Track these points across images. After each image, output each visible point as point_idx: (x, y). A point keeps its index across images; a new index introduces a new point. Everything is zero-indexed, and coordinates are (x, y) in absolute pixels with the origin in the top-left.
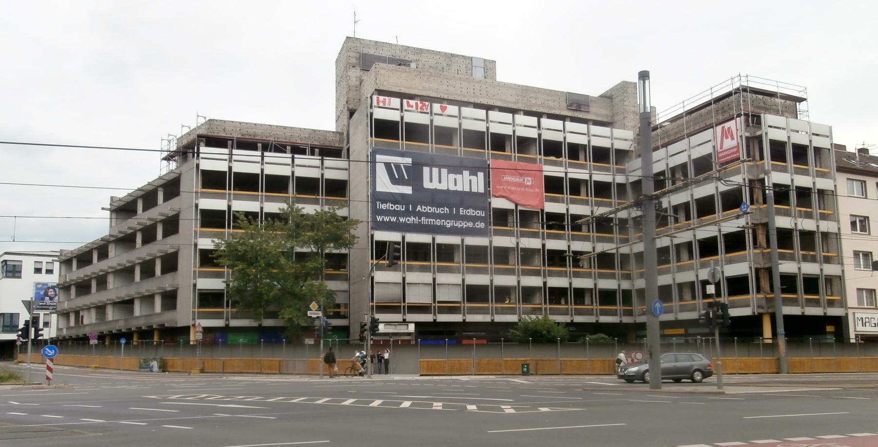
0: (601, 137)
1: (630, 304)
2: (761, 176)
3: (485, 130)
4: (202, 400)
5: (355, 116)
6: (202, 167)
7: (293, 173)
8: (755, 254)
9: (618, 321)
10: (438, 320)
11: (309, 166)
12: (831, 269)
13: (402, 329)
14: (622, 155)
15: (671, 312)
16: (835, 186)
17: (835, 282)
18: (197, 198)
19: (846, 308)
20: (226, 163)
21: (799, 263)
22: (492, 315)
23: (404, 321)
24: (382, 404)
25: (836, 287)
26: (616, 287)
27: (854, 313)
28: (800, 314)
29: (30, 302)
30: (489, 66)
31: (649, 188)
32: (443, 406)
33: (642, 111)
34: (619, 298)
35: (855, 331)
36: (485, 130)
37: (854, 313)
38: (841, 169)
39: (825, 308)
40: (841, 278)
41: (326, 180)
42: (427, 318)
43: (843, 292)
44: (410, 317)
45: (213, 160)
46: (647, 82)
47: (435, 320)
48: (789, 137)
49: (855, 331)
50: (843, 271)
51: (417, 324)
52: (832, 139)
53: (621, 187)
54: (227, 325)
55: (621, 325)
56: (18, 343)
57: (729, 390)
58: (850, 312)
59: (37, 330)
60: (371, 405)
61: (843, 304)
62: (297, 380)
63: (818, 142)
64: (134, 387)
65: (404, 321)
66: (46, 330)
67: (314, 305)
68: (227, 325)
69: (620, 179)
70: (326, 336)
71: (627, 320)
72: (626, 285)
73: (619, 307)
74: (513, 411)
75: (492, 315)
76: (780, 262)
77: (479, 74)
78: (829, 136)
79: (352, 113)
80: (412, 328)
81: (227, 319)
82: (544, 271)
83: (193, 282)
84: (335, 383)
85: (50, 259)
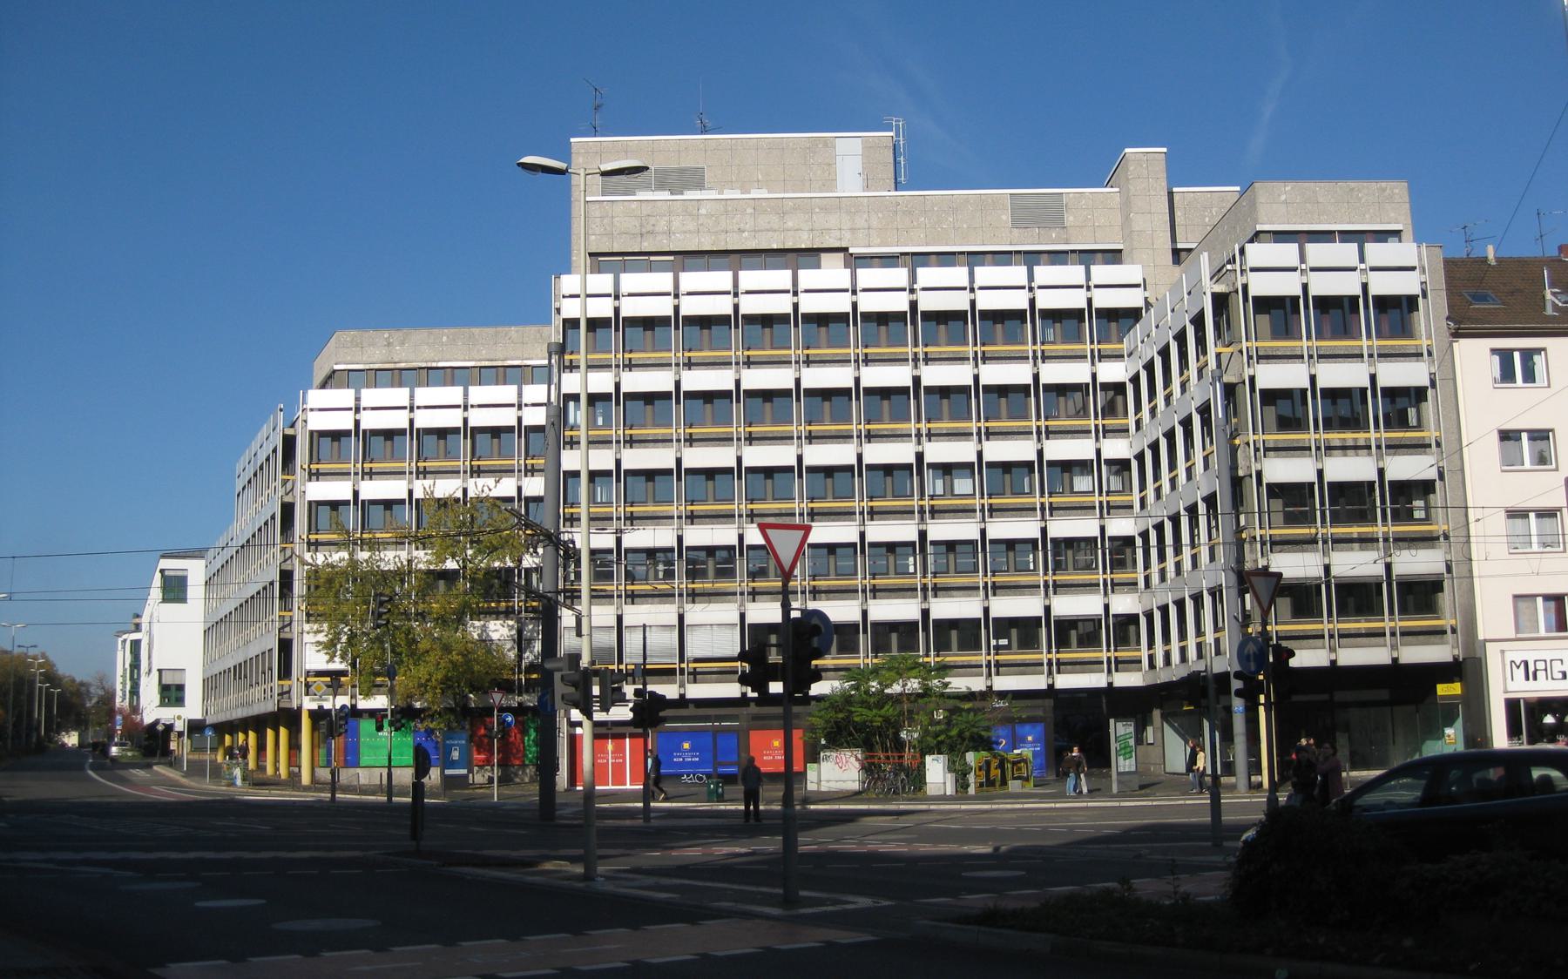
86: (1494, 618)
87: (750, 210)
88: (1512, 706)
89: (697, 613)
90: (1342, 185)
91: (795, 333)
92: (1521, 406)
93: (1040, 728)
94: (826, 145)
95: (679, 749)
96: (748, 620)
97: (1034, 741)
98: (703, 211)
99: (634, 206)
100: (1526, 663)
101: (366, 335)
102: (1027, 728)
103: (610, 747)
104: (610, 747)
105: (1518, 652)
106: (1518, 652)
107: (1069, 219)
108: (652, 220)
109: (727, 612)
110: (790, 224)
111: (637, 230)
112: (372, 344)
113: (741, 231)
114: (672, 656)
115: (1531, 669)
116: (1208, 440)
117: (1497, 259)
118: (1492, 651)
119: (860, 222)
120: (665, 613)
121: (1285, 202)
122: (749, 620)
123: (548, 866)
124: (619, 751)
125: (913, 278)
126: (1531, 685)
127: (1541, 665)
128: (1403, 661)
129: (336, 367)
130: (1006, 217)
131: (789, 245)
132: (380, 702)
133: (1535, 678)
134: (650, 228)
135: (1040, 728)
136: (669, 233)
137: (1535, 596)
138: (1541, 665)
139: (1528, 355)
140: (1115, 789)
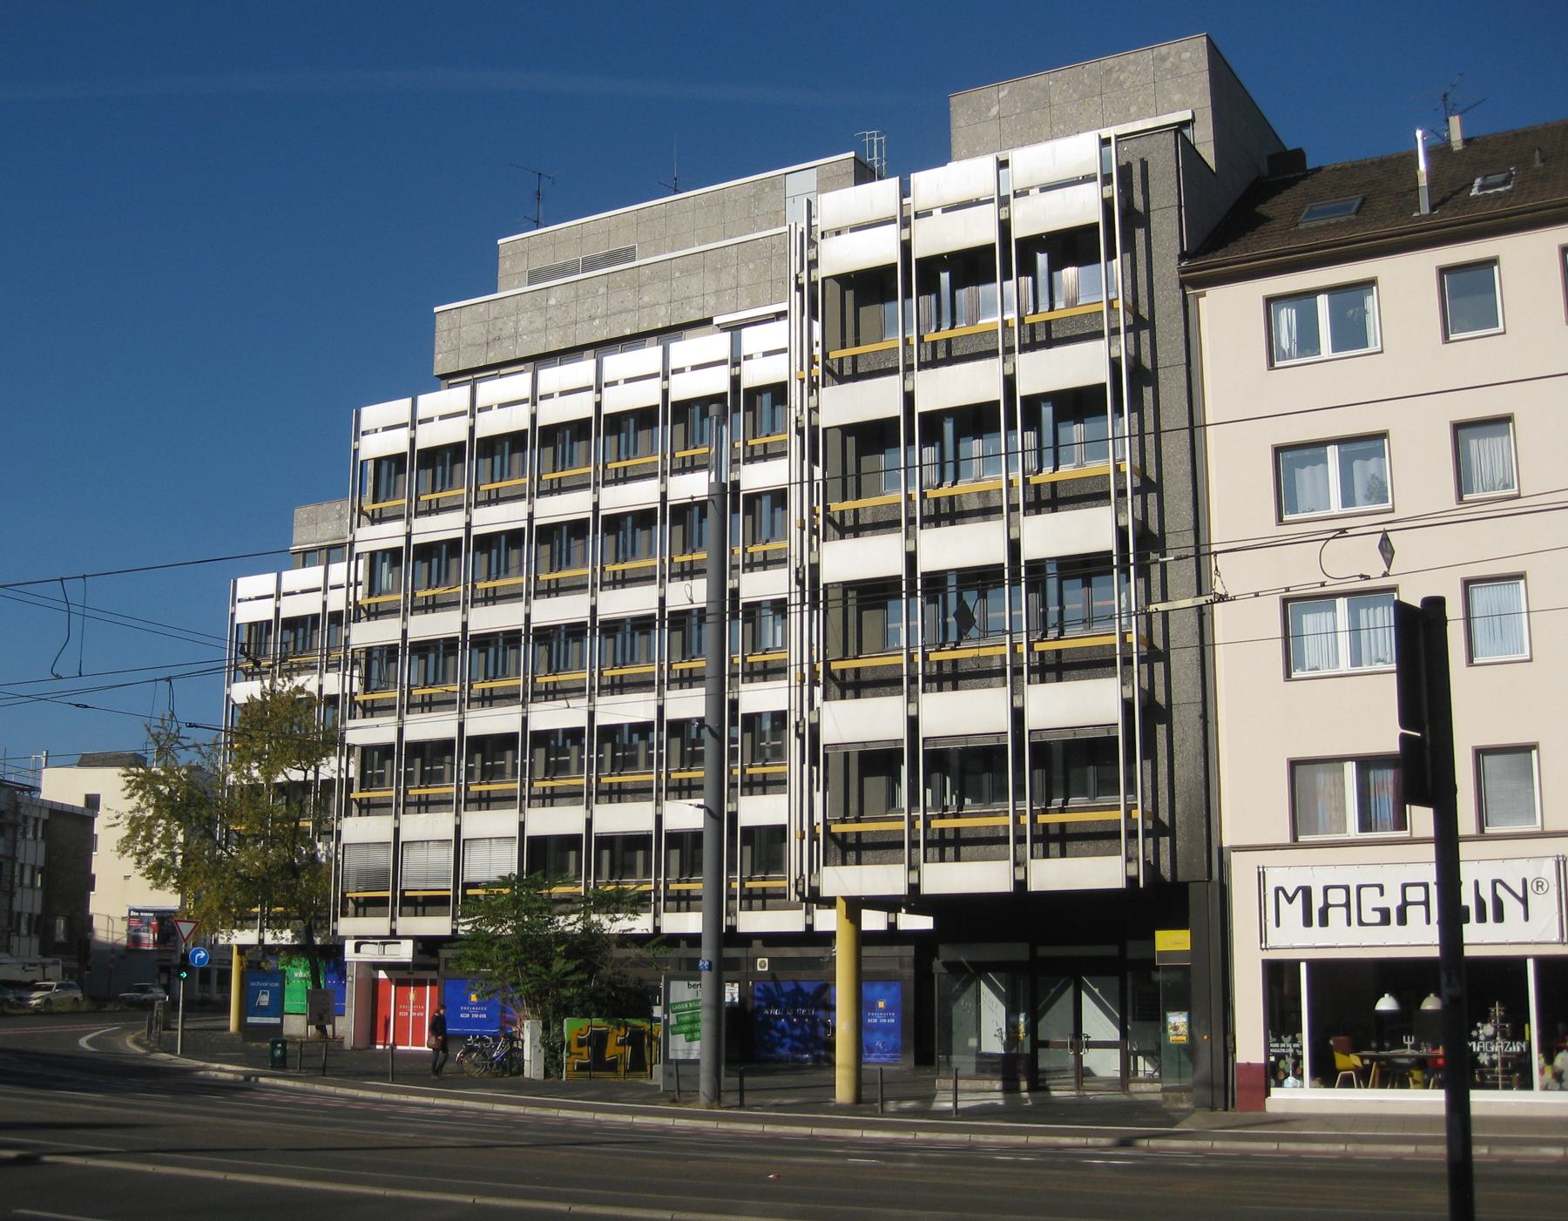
86: (1250, 806)
87: (602, 290)
88: (1278, 975)
89: (478, 823)
90: (1093, 67)
91: (598, 442)
92: (1327, 393)
93: (894, 989)
94: (773, 187)
95: (466, 1002)
96: (529, 832)
97: (886, 1010)
98: (552, 302)
99: (481, 309)
100: (1307, 892)
101: (320, 508)
102: (878, 988)
103: (412, 996)
104: (412, 996)
105: (1288, 872)
106: (1288, 872)
108: (499, 323)
109: (501, 822)
110: (646, 299)
111: (483, 340)
112: (325, 519)
113: (592, 318)
114: (448, 880)
115: (1317, 903)
116: (1350, 532)
117: (1467, 141)
118: (1242, 873)
119: (727, 280)
120: (438, 824)
121: (999, 117)
122: (531, 831)
123: (1104, 1141)
124: (420, 1001)
125: (735, 344)
126: (1316, 935)
127: (1337, 897)
128: (1034, 886)
131: (645, 327)
132: (286, 937)
133: (1324, 921)
134: (497, 333)
135: (894, 989)
136: (516, 336)
137: (1342, 759)
138: (1337, 897)
139: (1351, 296)
140: (843, 1091)
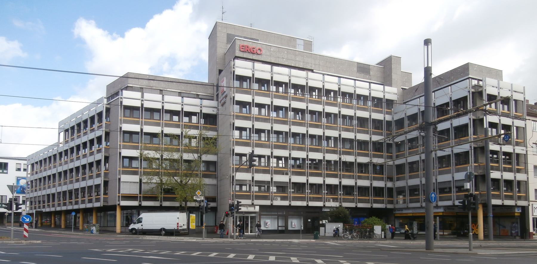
0: (377, 91)
1: (392, 197)
2: (481, 117)
3: (305, 84)
4: (130, 253)
5: (222, 73)
6: (124, 104)
7: (182, 109)
8: (475, 166)
9: (384, 207)
10: (274, 204)
11: (246, 68)
12: (521, 177)
13: (251, 209)
14: (390, 103)
15: (450, 200)
16: (526, 124)
17: (522, 186)
18: (121, 123)
19: (529, 201)
20: (140, 101)
21: (502, 172)
22: (308, 202)
23: (253, 204)
24: (229, 255)
25: (522, 188)
26: (384, 186)
27: (532, 204)
28: (501, 204)
29: (12, 186)
30: (308, 44)
31: (433, 117)
32: (276, 259)
33: (426, 66)
34: (385, 192)
35: (533, 215)
36: (305, 84)
37: (532, 204)
38: (529, 114)
39: (516, 201)
40: (526, 183)
41: (203, 114)
42: (267, 203)
43: (527, 191)
44: (256, 202)
45: (131, 98)
46: (430, 47)
47: (272, 204)
48: (499, 93)
49: (533, 215)
50: (528, 178)
51: (261, 207)
52: (524, 95)
53: (389, 123)
54: (140, 205)
55: (386, 209)
56: (6, 214)
57: (474, 251)
58: (531, 203)
59: (17, 205)
60: (210, 256)
61: (527, 198)
62: (190, 240)
63: (516, 96)
64: (83, 243)
65: (253, 204)
66: (23, 207)
67: (198, 192)
68: (140, 205)
69: (388, 118)
70: (207, 212)
71: (389, 206)
72: (390, 185)
73: (386, 198)
74: (298, 261)
75: (308, 202)
76: (491, 171)
77: (300, 48)
78: (523, 93)
79: (220, 71)
80: (257, 209)
81: (140, 201)
82: (340, 175)
83: (118, 177)
84: (214, 243)
85: (25, 162)
87: (286, 52)
98: (272, 50)
107: (371, 73)
110: (297, 59)
129: (129, 85)
130: (355, 69)
